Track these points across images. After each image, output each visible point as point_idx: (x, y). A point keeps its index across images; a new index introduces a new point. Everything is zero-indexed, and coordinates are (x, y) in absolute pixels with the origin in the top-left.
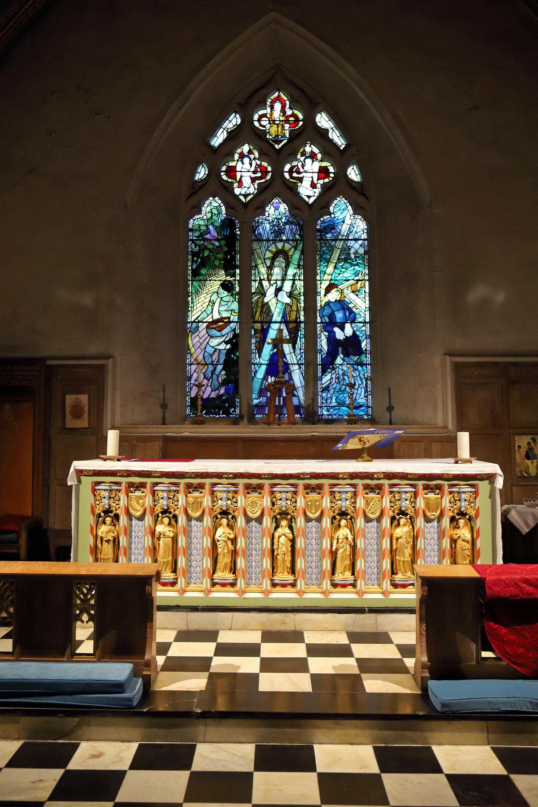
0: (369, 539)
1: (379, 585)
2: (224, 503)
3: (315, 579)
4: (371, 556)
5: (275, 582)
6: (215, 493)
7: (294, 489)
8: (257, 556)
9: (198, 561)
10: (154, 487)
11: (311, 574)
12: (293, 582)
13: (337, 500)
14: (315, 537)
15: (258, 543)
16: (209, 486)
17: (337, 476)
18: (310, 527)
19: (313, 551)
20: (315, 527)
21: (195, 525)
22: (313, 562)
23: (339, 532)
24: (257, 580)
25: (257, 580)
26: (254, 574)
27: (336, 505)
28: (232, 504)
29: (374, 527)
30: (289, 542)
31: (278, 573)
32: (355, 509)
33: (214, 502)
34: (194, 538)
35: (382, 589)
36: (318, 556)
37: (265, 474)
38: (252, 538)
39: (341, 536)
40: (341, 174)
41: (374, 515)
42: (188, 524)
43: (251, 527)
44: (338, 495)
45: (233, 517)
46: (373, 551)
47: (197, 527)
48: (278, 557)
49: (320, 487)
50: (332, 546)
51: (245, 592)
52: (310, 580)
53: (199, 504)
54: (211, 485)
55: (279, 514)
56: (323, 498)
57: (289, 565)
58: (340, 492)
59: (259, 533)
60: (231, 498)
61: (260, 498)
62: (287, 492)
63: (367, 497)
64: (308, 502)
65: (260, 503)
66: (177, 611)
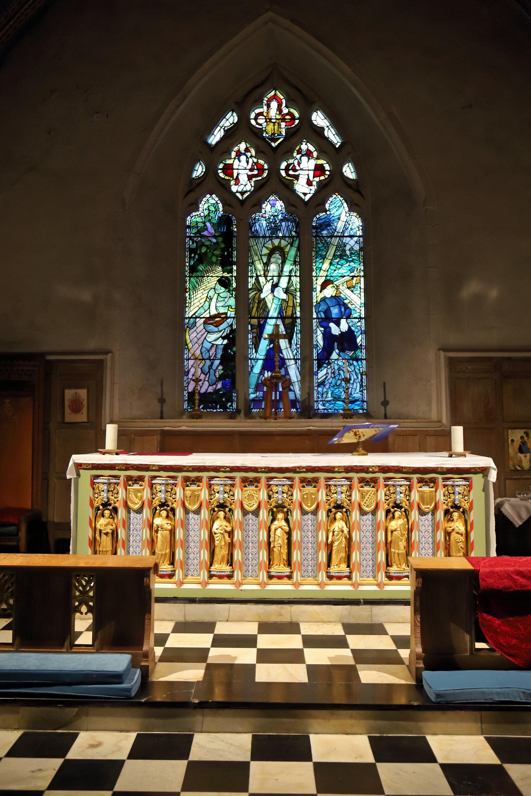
0: (365, 532)
1: (374, 577)
2: (222, 496)
3: (311, 571)
4: (366, 549)
5: (271, 574)
6: (212, 486)
7: (290, 483)
8: (254, 549)
9: (195, 553)
10: (152, 480)
11: (307, 566)
12: (289, 574)
13: (333, 493)
14: (311, 530)
15: (254, 535)
16: (207, 480)
17: (332, 469)
18: (306, 520)
19: (309, 543)
20: (311, 520)
21: (193, 517)
22: (309, 555)
23: (335, 525)
24: (254, 572)
25: (254, 572)
26: (250, 566)
27: (332, 498)
28: (228, 497)
29: (369, 520)
30: (285, 534)
31: (274, 565)
32: (351, 502)
33: (211, 495)
34: (191, 530)
35: (377, 581)
36: (314, 549)
37: (261, 468)
38: (249, 531)
39: (336, 529)
40: (337, 172)
41: (369, 508)
42: (186, 517)
43: (247, 519)
44: (333, 488)
45: (230, 510)
46: (368, 544)
47: (194, 519)
48: (275, 549)
49: (315, 481)
50: (327, 538)
51: (242, 584)
52: (306, 572)
53: (197, 497)
54: (209, 478)
55: (275, 507)
56: (318, 491)
57: (285, 557)
58: (335, 486)
59: (256, 525)
60: (228, 491)
61: (256, 491)
62: (283, 485)
63: (363, 491)
64: (304, 495)
65: (257, 496)
66: (175, 603)
